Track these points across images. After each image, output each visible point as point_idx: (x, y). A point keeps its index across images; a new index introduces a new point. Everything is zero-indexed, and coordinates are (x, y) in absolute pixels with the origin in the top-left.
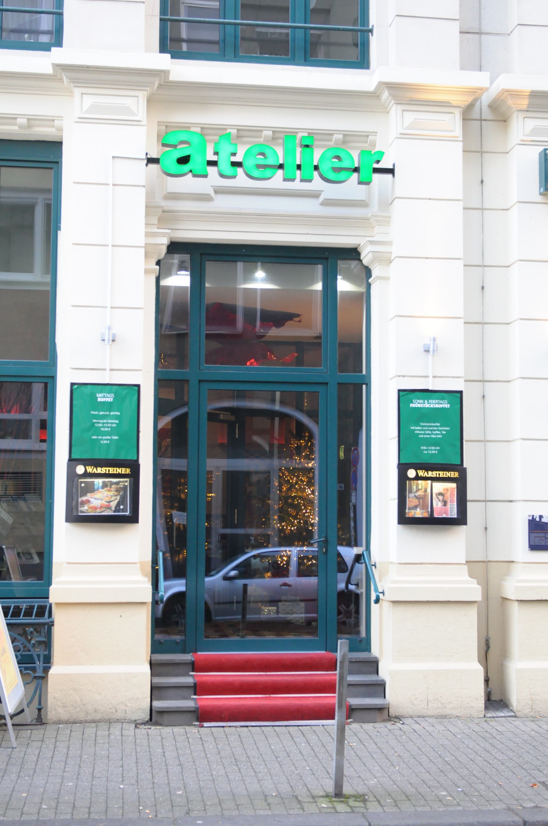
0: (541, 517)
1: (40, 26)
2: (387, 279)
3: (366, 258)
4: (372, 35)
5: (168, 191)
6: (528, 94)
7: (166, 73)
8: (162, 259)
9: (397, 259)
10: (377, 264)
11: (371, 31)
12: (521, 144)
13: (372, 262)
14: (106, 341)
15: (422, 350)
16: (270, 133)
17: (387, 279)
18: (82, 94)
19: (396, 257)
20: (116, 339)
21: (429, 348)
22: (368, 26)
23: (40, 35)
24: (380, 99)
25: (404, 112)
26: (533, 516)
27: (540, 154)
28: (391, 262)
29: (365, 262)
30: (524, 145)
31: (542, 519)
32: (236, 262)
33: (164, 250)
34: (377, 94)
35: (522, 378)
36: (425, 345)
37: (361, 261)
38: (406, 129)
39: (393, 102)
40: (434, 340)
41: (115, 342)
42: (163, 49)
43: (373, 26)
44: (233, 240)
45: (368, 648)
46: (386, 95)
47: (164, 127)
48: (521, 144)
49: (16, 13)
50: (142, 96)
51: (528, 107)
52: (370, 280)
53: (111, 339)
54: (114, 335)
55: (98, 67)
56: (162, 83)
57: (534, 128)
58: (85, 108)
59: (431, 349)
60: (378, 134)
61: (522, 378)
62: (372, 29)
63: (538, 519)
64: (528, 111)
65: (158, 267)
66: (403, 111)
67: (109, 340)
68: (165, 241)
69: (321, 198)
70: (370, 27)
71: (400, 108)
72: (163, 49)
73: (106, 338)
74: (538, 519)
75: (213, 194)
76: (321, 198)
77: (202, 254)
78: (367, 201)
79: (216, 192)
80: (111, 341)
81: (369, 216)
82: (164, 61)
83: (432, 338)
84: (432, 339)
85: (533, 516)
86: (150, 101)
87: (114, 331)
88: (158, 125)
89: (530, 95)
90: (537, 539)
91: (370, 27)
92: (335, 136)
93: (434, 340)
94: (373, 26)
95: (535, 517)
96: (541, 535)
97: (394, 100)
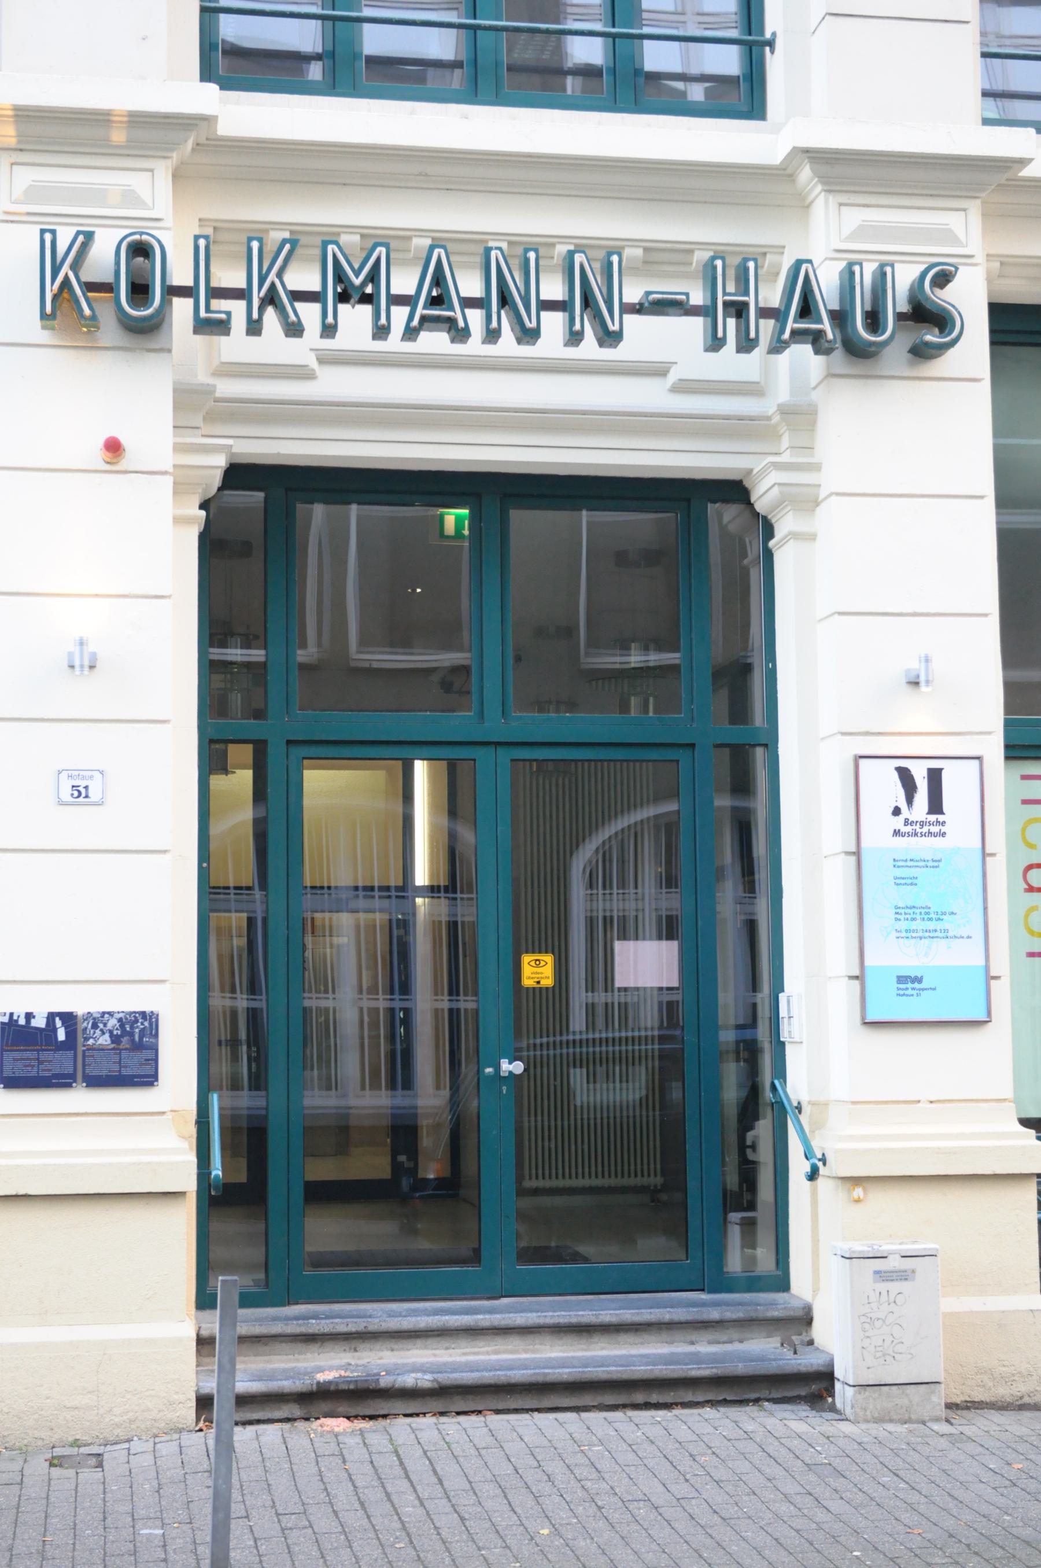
0: (29, 1016)
1: (362, 46)
2: (812, 537)
3: (763, 498)
4: (772, 52)
5: (224, 359)
6: (125, 119)
7: (209, 120)
8: (214, 497)
9: (834, 498)
10: (789, 508)
11: (771, 43)
12: (7, 221)
13: (778, 504)
14: (77, 669)
15: (904, 681)
16: (639, 252)
17: (812, 537)
18: (12, 164)
19: (831, 494)
20: (98, 665)
21: (918, 677)
22: (761, 31)
23: (313, 62)
24: (794, 181)
25: (14, 167)
26: (11, 1014)
27: (841, 273)
28: (818, 505)
29: (759, 507)
30: (12, 222)
31: (33, 1021)
32: (350, 503)
33: (217, 480)
34: (789, 171)
35: (844, 734)
36: (907, 671)
37: (752, 505)
38: (16, 202)
39: (819, 188)
40: (927, 660)
41: (95, 670)
42: (207, 74)
43: (774, 34)
44: (528, 463)
45: (783, 1284)
46: (805, 173)
47: (998, 265)
48: (7, 221)
49: (436, 29)
50: (163, 170)
51: (19, 142)
52: (771, 544)
53: (86, 663)
54: (94, 657)
55: (167, 116)
56: (203, 141)
57: (861, 225)
58: (846, 231)
59: (922, 679)
60: (786, 251)
61: (844, 734)
62: (774, 40)
63: (22, 1022)
64: (21, 150)
65: (203, 513)
66: (841, 205)
67: (82, 666)
68: (221, 461)
69: (673, 377)
70: (768, 35)
71: (833, 200)
72: (207, 74)
73: (77, 663)
74: (22, 1022)
75: (313, 364)
76: (673, 377)
77: (288, 490)
78: (763, 383)
79: (321, 361)
80: (86, 669)
81: (770, 414)
82: (207, 99)
83: (923, 656)
84: (923, 659)
85: (11, 1014)
86: (178, 176)
87: (91, 648)
88: (200, 226)
89: (129, 122)
90: (19, 1064)
91: (768, 35)
92: (416, 241)
93: (81, 643)
94: (774, 34)
95: (15, 1018)
96: (28, 1054)
97: (823, 183)
